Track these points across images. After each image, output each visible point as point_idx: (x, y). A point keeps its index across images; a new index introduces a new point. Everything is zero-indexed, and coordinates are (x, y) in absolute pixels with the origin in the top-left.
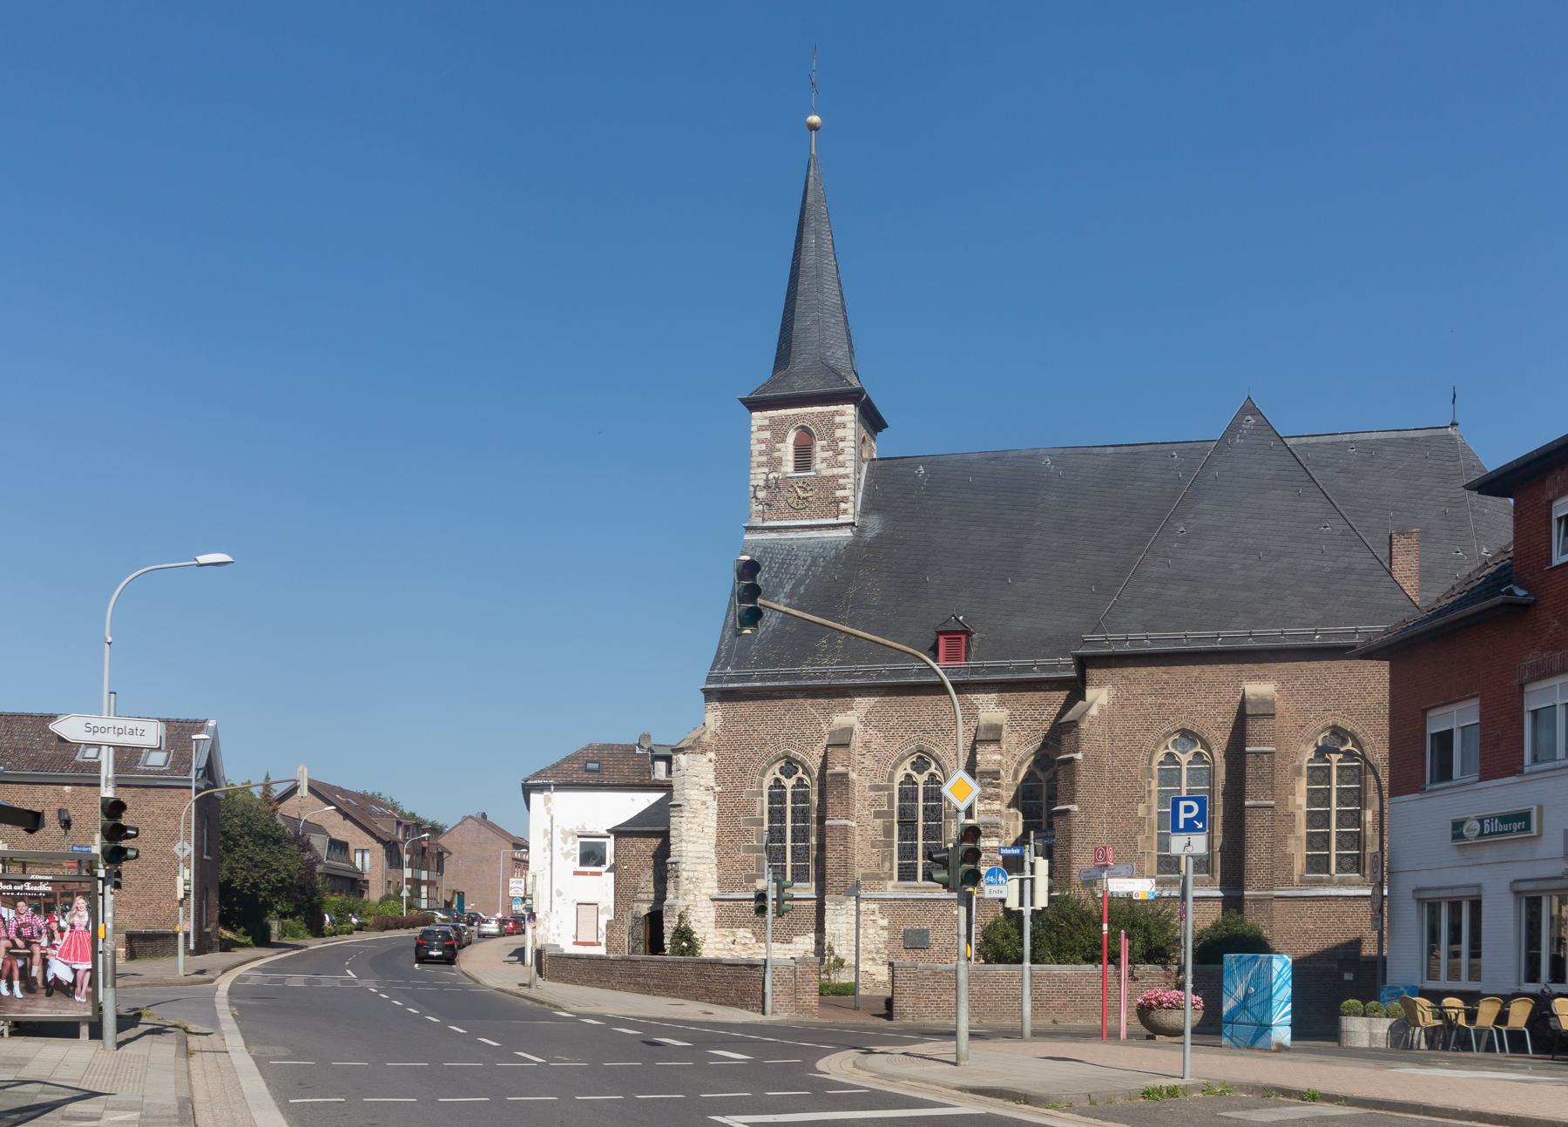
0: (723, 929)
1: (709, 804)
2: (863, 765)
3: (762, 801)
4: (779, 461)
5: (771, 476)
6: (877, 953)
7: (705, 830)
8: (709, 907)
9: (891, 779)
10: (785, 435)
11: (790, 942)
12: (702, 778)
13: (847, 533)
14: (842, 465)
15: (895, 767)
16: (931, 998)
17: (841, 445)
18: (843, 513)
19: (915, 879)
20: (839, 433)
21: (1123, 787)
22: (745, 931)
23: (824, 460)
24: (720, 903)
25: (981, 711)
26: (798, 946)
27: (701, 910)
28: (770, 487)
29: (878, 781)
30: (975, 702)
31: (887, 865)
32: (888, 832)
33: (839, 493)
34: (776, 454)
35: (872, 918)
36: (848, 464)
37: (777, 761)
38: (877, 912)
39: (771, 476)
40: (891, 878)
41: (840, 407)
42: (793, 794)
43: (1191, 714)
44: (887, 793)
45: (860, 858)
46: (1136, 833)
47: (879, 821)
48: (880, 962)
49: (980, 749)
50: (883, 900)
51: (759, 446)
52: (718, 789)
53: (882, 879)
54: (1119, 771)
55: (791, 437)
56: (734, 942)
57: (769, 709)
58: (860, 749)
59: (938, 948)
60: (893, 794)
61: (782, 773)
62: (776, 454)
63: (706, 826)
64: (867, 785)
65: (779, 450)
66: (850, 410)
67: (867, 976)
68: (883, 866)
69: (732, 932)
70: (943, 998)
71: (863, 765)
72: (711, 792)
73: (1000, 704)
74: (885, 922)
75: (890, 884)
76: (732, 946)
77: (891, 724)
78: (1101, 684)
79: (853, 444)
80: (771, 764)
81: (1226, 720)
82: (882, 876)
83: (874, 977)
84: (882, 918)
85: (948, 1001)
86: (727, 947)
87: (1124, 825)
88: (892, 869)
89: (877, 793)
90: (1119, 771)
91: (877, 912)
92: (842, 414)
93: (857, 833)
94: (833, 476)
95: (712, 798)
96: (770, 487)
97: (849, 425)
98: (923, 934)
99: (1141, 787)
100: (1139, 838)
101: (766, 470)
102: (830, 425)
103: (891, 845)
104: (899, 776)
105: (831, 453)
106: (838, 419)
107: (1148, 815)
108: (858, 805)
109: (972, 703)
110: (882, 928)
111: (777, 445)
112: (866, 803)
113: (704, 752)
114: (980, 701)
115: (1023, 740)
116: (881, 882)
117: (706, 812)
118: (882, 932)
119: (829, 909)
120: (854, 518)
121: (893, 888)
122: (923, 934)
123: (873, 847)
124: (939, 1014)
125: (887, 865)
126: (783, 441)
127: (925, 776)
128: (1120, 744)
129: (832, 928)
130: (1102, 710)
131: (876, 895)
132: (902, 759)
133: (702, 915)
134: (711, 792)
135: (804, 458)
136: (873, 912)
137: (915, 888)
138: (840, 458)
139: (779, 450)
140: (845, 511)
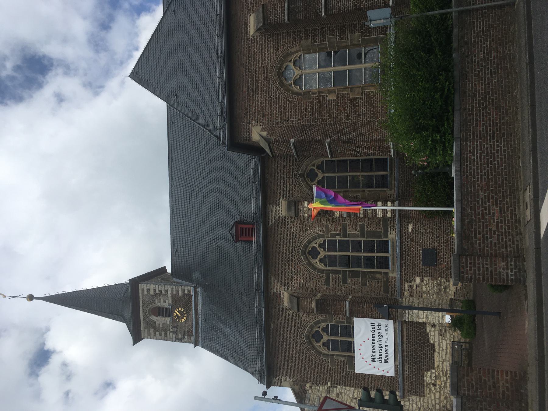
0: (425, 392)
1: (338, 392)
2: (314, 289)
3: (337, 355)
4: (164, 325)
5: (171, 330)
6: (441, 285)
7: (356, 396)
8: (409, 399)
9: (322, 271)
10: (152, 321)
11: (433, 345)
12: (321, 395)
13: (199, 290)
14: (167, 291)
15: (315, 268)
16: (495, 241)
17: (157, 292)
18: (190, 292)
19: (387, 258)
20: (152, 292)
21: (316, 111)
22: (426, 376)
23: (164, 301)
24: (406, 391)
25: (281, 215)
26: (436, 340)
27: (411, 407)
28: (177, 331)
29: (324, 280)
30: (276, 219)
31: (378, 276)
32: (355, 275)
33: (180, 293)
34: (161, 326)
35: (415, 287)
36: (166, 289)
37: (312, 344)
38: (410, 284)
39: (171, 330)
40: (387, 273)
41: (140, 292)
42: (332, 335)
43: (267, 69)
44: (331, 275)
45: (373, 294)
46: (348, 99)
47: (349, 280)
48: (447, 283)
49: (258, 159)
50: (402, 278)
51: (157, 336)
52: (329, 384)
53: (387, 279)
54: (305, 115)
55: (154, 318)
56: (435, 385)
57: (280, 346)
58: (304, 290)
59: (436, 243)
60: (332, 270)
61: (319, 341)
62: (161, 326)
63: (353, 395)
64: (326, 287)
65: (159, 325)
66: (141, 286)
67: (458, 293)
68: (379, 279)
69: (427, 386)
70: (494, 229)
71: (314, 289)
72: (331, 389)
73: (277, 203)
74: (418, 280)
75: (391, 275)
76: (438, 386)
77: (289, 270)
78: (250, 132)
79: (157, 286)
80: (314, 347)
81: (272, 46)
82: (385, 279)
83: (458, 288)
84: (415, 281)
85: (497, 223)
86: (438, 390)
87: (342, 109)
88: (380, 273)
89: (331, 281)
90: (305, 115)
91: (410, 284)
92: (143, 290)
93: (357, 295)
94: (172, 296)
95: (335, 389)
96: (177, 331)
97: (149, 287)
98: (425, 252)
99: (316, 99)
100: (351, 97)
101: (168, 332)
102: (149, 298)
103: (364, 272)
104: (321, 266)
105: (161, 297)
106: (146, 293)
107: (335, 92)
108: (338, 293)
109: (276, 221)
110: (422, 281)
111: (157, 325)
112: (337, 288)
113: (305, 391)
114: (275, 215)
115: (298, 189)
116: (390, 280)
117: (343, 394)
118: (425, 282)
119: (408, 318)
120: (192, 286)
121: (395, 274)
122: (425, 252)
123: (366, 285)
124: (515, 233)
125: (378, 276)
126: (155, 322)
127: (320, 250)
128: (287, 115)
129: (422, 317)
130: (263, 130)
131: (398, 284)
132: (310, 264)
133: (415, 406)
134: (331, 389)
135: (163, 312)
136: (411, 287)
137: (393, 258)
138: (163, 292)
139: (159, 325)
140: (189, 291)
